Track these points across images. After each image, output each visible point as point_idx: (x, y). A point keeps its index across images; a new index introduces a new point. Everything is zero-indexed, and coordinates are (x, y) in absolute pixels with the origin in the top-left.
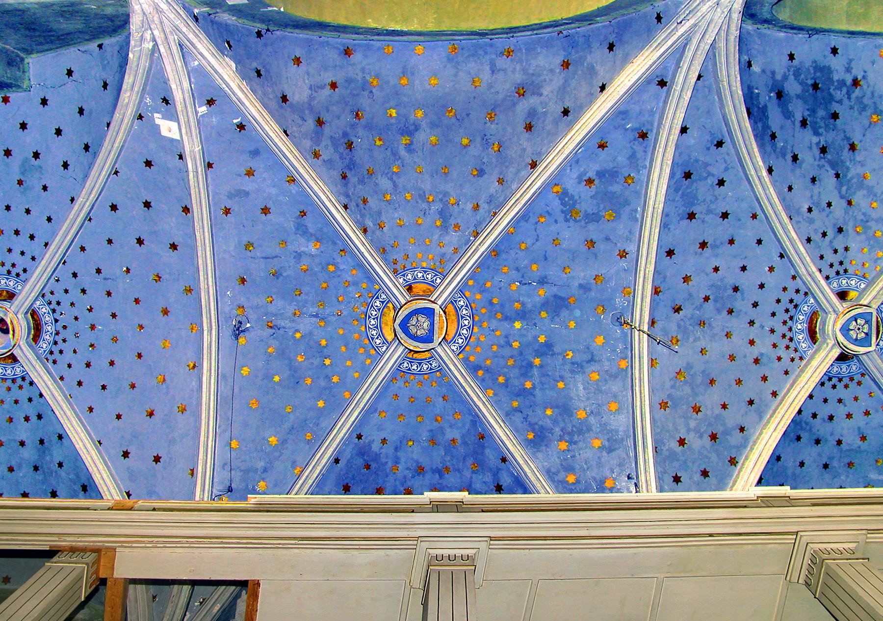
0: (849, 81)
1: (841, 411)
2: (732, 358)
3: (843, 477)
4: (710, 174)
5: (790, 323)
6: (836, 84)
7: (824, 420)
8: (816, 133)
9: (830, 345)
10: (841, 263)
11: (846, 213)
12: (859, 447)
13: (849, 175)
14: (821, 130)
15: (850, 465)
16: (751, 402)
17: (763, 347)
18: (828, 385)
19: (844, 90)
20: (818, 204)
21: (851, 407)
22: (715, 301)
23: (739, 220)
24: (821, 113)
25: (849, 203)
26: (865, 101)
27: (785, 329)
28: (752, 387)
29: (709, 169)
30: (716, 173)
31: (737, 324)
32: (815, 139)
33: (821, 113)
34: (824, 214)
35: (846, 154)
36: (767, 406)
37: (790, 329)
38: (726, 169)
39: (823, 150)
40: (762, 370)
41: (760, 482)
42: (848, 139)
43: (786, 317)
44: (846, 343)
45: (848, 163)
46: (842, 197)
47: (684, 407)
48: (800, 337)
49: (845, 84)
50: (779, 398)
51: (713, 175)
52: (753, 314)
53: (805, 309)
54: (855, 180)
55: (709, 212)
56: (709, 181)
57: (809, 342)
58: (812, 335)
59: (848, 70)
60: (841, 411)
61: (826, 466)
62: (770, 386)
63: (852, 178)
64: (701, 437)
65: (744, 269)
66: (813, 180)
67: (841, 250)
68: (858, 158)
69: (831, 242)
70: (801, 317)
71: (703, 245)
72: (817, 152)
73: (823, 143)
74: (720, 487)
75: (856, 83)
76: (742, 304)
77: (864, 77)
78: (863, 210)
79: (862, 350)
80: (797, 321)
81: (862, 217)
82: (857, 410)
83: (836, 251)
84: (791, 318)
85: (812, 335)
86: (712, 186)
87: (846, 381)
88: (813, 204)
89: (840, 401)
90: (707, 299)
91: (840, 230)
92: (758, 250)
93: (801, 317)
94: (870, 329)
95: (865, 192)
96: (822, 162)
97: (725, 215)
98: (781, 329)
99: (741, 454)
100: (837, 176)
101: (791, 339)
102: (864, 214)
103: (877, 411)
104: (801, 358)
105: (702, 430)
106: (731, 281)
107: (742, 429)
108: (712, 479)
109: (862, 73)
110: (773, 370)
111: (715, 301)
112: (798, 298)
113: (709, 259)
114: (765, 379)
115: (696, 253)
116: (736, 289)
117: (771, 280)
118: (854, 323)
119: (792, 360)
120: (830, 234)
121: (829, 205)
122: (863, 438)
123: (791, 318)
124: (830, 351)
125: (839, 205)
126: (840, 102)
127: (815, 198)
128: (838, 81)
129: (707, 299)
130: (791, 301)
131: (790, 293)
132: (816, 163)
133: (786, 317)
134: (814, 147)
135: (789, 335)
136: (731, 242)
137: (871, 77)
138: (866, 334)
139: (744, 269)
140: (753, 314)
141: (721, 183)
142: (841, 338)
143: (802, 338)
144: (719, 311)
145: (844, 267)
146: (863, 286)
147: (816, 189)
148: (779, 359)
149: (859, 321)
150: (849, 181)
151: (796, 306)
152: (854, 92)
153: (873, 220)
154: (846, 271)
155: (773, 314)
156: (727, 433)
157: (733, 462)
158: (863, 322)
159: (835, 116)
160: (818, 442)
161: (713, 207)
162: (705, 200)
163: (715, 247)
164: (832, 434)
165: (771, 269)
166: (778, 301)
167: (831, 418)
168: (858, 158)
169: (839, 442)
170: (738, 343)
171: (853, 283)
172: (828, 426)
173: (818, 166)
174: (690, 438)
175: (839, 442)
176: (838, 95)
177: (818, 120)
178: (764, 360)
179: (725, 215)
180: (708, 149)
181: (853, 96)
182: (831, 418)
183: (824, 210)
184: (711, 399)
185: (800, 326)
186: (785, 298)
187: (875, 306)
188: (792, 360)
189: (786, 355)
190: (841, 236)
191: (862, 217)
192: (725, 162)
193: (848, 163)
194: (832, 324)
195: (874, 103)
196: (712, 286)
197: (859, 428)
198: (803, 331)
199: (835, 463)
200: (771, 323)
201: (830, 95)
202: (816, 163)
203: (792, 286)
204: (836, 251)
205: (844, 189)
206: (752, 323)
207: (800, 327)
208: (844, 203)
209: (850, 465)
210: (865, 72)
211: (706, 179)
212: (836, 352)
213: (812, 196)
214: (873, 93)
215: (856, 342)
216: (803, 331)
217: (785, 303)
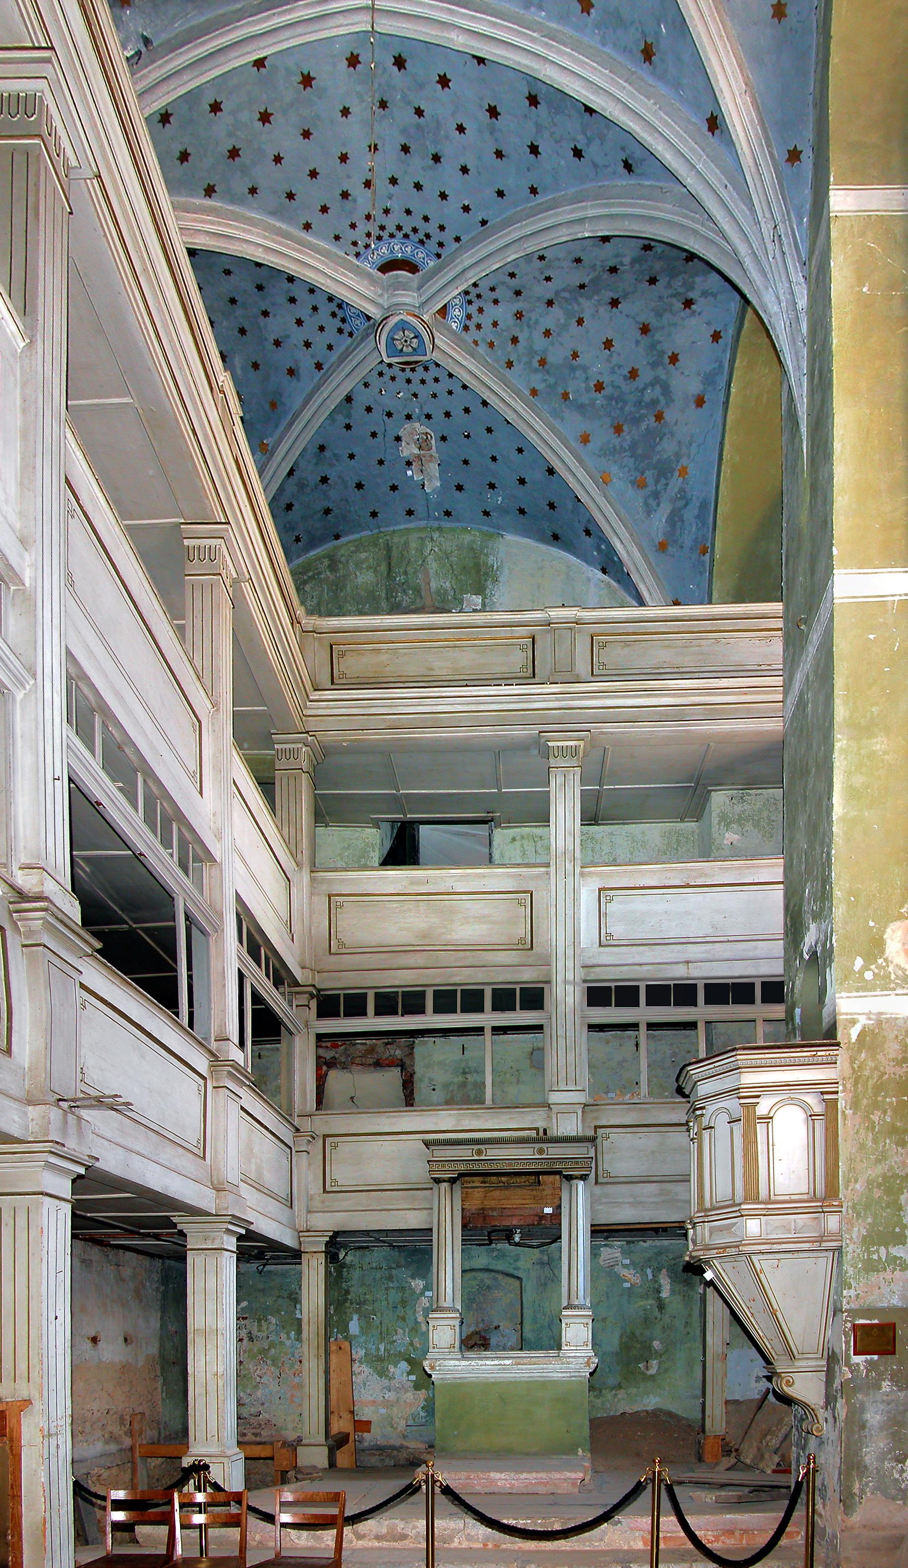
0: (691, 295)
1: (304, 311)
2: (344, 158)
3: (225, 323)
4: (589, 141)
5: (400, 235)
6: (690, 280)
7: (288, 291)
8: (633, 262)
9: (380, 301)
10: (479, 296)
11: (539, 299)
12: (266, 339)
13: (582, 300)
14: (637, 265)
15: (243, 331)
16: (291, 196)
17: (362, 199)
18: (333, 307)
19: (681, 290)
20: (549, 267)
21: (311, 323)
22: (418, 127)
23: (529, 170)
24: (658, 266)
25: (550, 303)
26: (667, 316)
27: (391, 228)
28: (312, 194)
29: (598, 141)
30: (590, 150)
31: (388, 161)
32: (627, 260)
33: (658, 266)
34: (537, 274)
35: (607, 295)
36: (290, 221)
37: (392, 236)
38: (595, 166)
39: (613, 270)
40: (335, 204)
41: (192, 253)
42: (625, 296)
43: (407, 229)
44: (387, 329)
45: (596, 298)
46: (557, 293)
47: (265, 97)
48: (384, 250)
49: (688, 290)
50: (303, 235)
51: (588, 145)
52: (406, 183)
53: (420, 255)
54: (576, 307)
55: (539, 128)
56: (580, 137)
57: (380, 262)
58: (387, 267)
59: (705, 294)
60: (304, 311)
61: (233, 301)
62: (316, 218)
63: (579, 304)
64: (231, 135)
65: (465, 170)
66: (578, 261)
67: (494, 295)
68: (601, 310)
69: (503, 283)
70: (409, 249)
71: (493, 112)
72: (611, 263)
73: (622, 268)
74: (172, 186)
75: (688, 303)
76: (417, 167)
77: (694, 312)
78: (542, 320)
79: (382, 347)
80: (403, 244)
81: (533, 319)
82: (309, 331)
83: (493, 289)
84: (406, 236)
85: (387, 267)
86: (575, 140)
87: (340, 314)
88: (550, 261)
89: (315, 309)
90: (419, 112)
91: (518, 293)
92: (491, 193)
93: (409, 249)
94: (408, 355)
95: (562, 321)
96: (599, 268)
97: (534, 150)
98: (391, 223)
99: (222, 199)
100: (582, 286)
101: (379, 238)
102: (537, 322)
103: (313, 356)
104: (358, 255)
105: (239, 133)
106: (446, 151)
107: (253, 191)
108: (180, 169)
109: (699, 310)
110: (337, 221)
111: (418, 127)
112: (432, 245)
113: (476, 120)
114: (324, 209)
115: (481, 99)
116: (436, 158)
117: (453, 206)
118: (412, 335)
119: (355, 244)
120: (513, 282)
121: (548, 279)
122: (277, 343)
123: (406, 236)
124: (373, 301)
125: (547, 290)
126: (669, 286)
127: (556, 263)
128: (693, 282)
129: (419, 112)
130: (428, 236)
131: (437, 236)
132: (598, 263)
133: (407, 229)
134: (619, 259)
135: (385, 235)
136: (499, 154)
137: (694, 321)
138: (402, 350)
139: (465, 170)
140: (406, 183)
141: (578, 153)
142: (393, 321)
143: (384, 252)
144: (404, 131)
145: (474, 299)
146: (454, 326)
147: (567, 264)
148: (353, 226)
149: (415, 340)
150: (576, 300)
151: (422, 242)
152: (679, 301)
153: (531, 333)
154: (470, 302)
155: (408, 212)
156: (244, 170)
157: (210, 191)
158: (397, 343)
159: (653, 281)
160: (260, 288)
161: (546, 134)
162: (555, 125)
163: (493, 131)
164: (274, 304)
165: (466, 209)
166: (426, 219)
167: (292, 300)
168: (601, 310)
169: (265, 314)
170: (362, 162)
171: (457, 312)
172: (282, 300)
173: (595, 265)
174: (224, 117)
175: (265, 314)
176: (677, 283)
177: (649, 263)
178: (348, 204)
179: (534, 150)
180: (623, 149)
181: (674, 300)
182: (292, 300)
183: (542, 273)
184: (282, 136)
185: (399, 249)
186: (432, 228)
187: (436, 356)
188: (355, 244)
189: (359, 235)
190: (511, 294)
191: (533, 319)
192: (606, 166)
193: (596, 298)
194: (406, 297)
195: (663, 328)
196: (438, 123)
197: (288, 337)
198: (392, 252)
199: (239, 311)
200: (397, 207)
201: (677, 275)
202: (598, 263)
203: (447, 237)
204: (493, 289)
205: (566, 295)
206: (393, 181)
207: (396, 248)
208: (549, 296)
209: (243, 331)
210: (699, 314)
211: (584, 134)
212: (375, 313)
213: (559, 259)
214: (675, 325)
215: (391, 340)
216: (392, 252)
217: (424, 228)
